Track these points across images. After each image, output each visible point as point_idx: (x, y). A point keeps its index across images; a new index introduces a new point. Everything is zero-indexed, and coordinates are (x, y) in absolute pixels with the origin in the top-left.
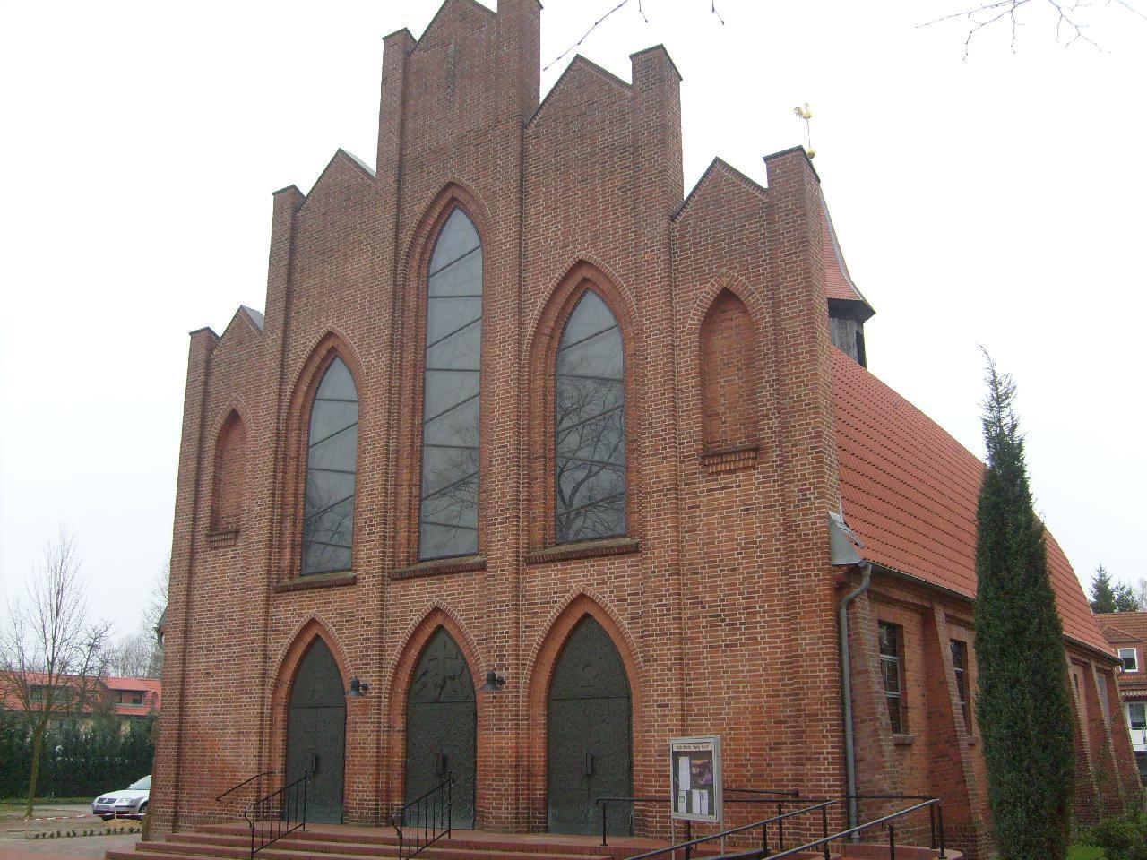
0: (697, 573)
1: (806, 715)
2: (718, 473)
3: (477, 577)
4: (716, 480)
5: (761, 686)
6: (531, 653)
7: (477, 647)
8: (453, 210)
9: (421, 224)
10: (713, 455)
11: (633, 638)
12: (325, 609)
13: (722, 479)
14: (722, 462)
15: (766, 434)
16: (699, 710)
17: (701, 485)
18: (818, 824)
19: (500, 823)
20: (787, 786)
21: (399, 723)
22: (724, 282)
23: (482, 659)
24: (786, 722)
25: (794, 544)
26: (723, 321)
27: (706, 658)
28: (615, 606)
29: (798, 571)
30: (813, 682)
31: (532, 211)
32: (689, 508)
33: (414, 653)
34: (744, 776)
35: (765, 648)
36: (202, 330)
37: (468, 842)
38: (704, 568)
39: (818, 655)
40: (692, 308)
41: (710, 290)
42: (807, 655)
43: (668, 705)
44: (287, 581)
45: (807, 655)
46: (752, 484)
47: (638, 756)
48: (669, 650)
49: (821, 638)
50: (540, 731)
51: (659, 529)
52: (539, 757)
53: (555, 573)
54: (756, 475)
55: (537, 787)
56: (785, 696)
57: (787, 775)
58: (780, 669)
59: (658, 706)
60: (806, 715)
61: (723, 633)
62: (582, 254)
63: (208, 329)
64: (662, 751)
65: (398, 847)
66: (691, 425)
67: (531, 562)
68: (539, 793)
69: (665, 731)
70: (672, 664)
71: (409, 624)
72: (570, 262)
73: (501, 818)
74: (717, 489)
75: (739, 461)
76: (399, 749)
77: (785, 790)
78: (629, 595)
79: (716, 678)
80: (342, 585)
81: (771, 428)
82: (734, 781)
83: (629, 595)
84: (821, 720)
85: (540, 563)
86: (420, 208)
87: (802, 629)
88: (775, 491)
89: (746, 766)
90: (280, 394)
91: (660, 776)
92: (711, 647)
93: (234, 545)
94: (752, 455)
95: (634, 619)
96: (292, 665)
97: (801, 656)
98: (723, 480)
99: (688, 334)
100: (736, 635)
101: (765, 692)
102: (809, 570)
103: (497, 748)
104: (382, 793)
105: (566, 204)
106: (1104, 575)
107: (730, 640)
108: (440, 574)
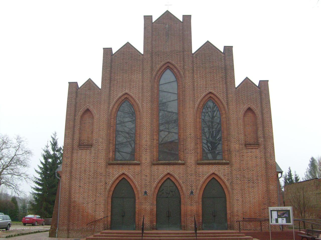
0: (244, 170)
1: (272, 203)
2: (249, 149)
3: (182, 167)
4: (248, 150)
5: (260, 196)
6: (199, 186)
7: (182, 184)
8: (167, 69)
9: (159, 71)
10: (247, 145)
11: (228, 184)
12: (129, 171)
13: (250, 150)
14: (251, 146)
15: (260, 141)
16: (245, 201)
17: (245, 151)
18: (238, 224)
19: (192, 228)
20: (266, 218)
21: (155, 203)
22: (249, 106)
23: (184, 187)
24: (266, 204)
25: (269, 166)
26: (246, 114)
27: (247, 190)
28: (223, 176)
29: (269, 172)
30: (273, 196)
31: (195, 76)
32: (242, 156)
33: (160, 185)
34: (256, 216)
35: (261, 188)
36: (74, 83)
37: (202, 233)
38: (246, 169)
39: (274, 190)
40: (241, 110)
41: (246, 107)
42: (272, 190)
43: (239, 200)
44: (111, 162)
45: (272, 190)
46: (257, 152)
47: (228, 211)
48: (239, 187)
49: (275, 187)
50: (201, 205)
51: (235, 159)
52: (201, 212)
53: (205, 168)
54: (258, 151)
55: (200, 219)
56: (266, 198)
57: (266, 215)
58: (264, 193)
59: (236, 200)
60: (272, 203)
61: (251, 184)
62: (211, 91)
63: (77, 83)
64: (238, 210)
65: (141, 235)
66: (242, 137)
67: (199, 164)
68: (201, 221)
69: (238, 206)
70: (240, 191)
71: (159, 177)
72: (207, 92)
73: (192, 227)
74: (249, 152)
75: (254, 147)
76: (155, 209)
77: (266, 218)
78: (227, 174)
79: (249, 194)
80: (135, 165)
81: (261, 140)
82: (254, 217)
83: (227, 174)
84: (275, 204)
85: (202, 164)
86: (158, 67)
87: (271, 184)
88: (263, 154)
89: (257, 213)
90: (109, 107)
91: (237, 216)
92: (248, 187)
93: (90, 149)
94: (258, 146)
95: (228, 180)
96: (114, 186)
97: (271, 190)
98: (250, 150)
99: (240, 116)
100: (254, 185)
101: (261, 197)
102: (272, 172)
103: (190, 209)
104: (151, 222)
105: (206, 77)
106: (296, 175)
107: (253, 186)
108: (170, 165)
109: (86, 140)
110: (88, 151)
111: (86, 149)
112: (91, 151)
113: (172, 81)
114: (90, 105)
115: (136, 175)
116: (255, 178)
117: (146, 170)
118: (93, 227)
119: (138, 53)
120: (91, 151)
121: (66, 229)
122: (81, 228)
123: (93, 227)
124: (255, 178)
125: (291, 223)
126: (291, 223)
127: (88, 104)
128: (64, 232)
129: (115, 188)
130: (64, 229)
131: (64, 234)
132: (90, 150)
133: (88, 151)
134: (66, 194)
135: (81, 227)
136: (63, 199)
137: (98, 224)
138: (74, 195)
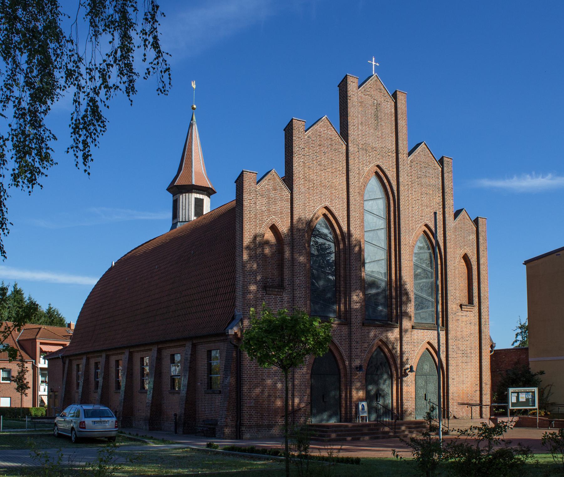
61: (465, 358)
109: (270, 279)
110: (278, 297)
111: (276, 295)
112: (283, 298)
113: (351, 162)
114: (277, 219)
115: (344, 340)
116: (469, 351)
117: (357, 334)
118: (290, 420)
119: (340, 140)
120: (283, 298)
121: (254, 424)
122: (274, 423)
123: (290, 420)
124: (469, 351)
125: (195, 198)
126: (195, 198)
127: (273, 216)
128: (253, 430)
129: (339, 370)
130: (251, 425)
131: (254, 432)
132: (281, 296)
133: (278, 297)
134: (253, 368)
135: (273, 421)
136: (247, 376)
137: (298, 415)
138: (261, 370)
